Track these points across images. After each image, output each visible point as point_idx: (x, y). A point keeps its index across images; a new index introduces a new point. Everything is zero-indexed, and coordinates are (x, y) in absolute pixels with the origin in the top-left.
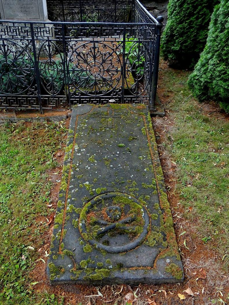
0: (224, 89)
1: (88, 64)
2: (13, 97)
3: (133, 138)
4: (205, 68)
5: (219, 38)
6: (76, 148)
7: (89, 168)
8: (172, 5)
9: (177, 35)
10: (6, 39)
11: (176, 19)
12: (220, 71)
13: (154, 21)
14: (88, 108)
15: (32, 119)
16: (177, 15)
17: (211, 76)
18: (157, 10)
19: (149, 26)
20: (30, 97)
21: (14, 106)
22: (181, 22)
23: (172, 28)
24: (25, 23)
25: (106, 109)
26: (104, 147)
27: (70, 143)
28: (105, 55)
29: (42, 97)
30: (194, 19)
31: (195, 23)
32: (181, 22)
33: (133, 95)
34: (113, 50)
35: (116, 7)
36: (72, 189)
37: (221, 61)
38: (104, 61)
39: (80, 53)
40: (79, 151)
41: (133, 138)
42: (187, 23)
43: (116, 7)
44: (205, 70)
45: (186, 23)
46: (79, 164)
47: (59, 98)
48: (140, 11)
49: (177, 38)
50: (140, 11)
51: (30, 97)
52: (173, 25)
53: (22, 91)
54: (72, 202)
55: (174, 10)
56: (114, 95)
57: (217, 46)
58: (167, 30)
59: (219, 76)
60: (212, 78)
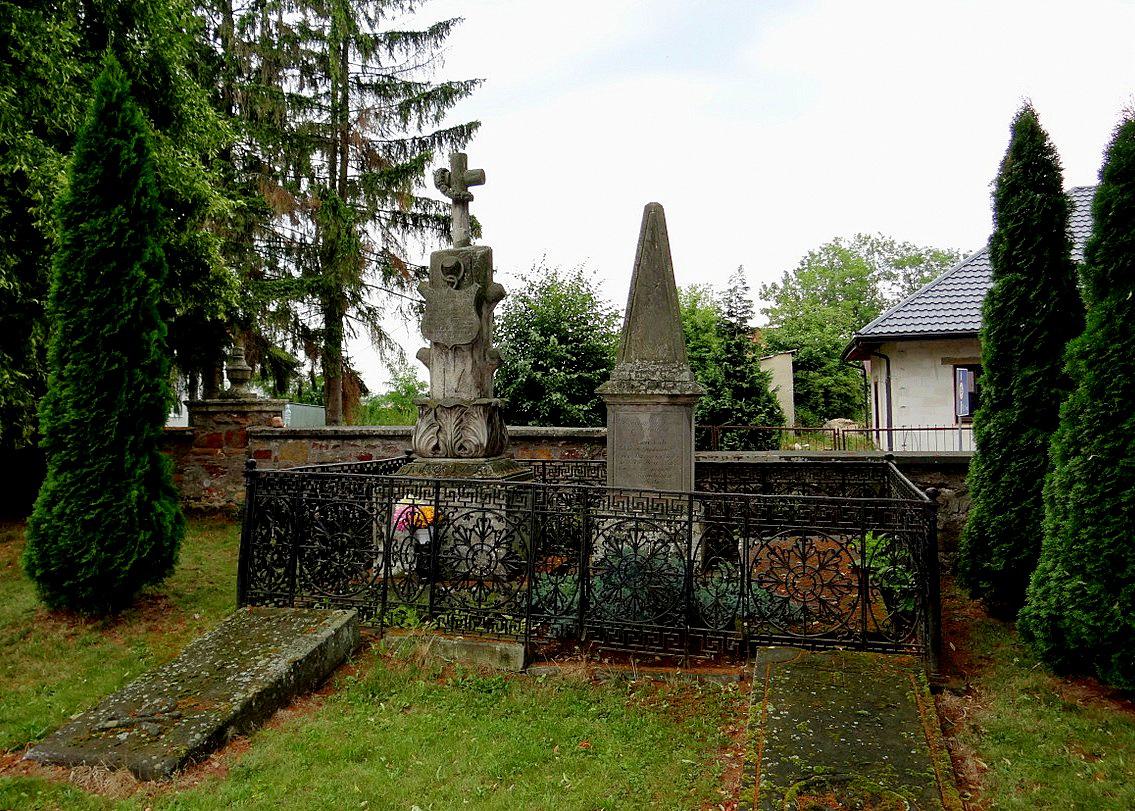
0: (1089, 627)
1: (789, 569)
2: (634, 627)
3: (888, 706)
4: (1043, 588)
5: (1062, 530)
6: (771, 708)
7: (798, 738)
8: (977, 478)
9: (992, 539)
10: (643, 520)
11: (988, 504)
12: (1072, 591)
13: (922, 498)
14: (791, 653)
15: (668, 675)
16: (989, 497)
17: (1058, 601)
18: (947, 490)
19: (910, 504)
20: (668, 630)
21: (633, 648)
22: (998, 510)
23: (981, 523)
24: (681, 495)
25: (828, 658)
26: (828, 714)
27: (756, 701)
28: (825, 554)
29: (692, 631)
30: (1030, 504)
31: (1034, 512)
32: (998, 510)
33: (887, 641)
34: (841, 545)
35: (844, 480)
36: (766, 762)
37: (1074, 571)
38: (823, 566)
39: (775, 549)
40: (776, 713)
41: (888, 706)
42: (1013, 511)
43: (844, 480)
44: (1043, 593)
45: (1011, 512)
46: (778, 732)
47: (726, 635)
48: (899, 486)
49: (994, 546)
50: (899, 486)
51: (668, 630)
52: (983, 517)
53: (656, 615)
54: (768, 778)
55: (981, 486)
56: (844, 638)
57: (1060, 544)
58: (970, 528)
59: (1072, 601)
60: (1060, 607)
